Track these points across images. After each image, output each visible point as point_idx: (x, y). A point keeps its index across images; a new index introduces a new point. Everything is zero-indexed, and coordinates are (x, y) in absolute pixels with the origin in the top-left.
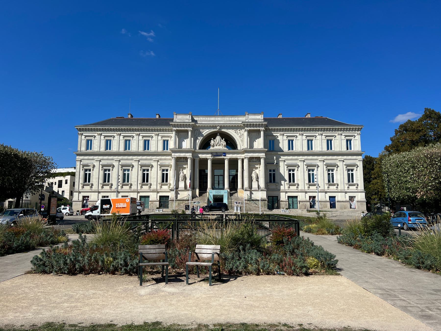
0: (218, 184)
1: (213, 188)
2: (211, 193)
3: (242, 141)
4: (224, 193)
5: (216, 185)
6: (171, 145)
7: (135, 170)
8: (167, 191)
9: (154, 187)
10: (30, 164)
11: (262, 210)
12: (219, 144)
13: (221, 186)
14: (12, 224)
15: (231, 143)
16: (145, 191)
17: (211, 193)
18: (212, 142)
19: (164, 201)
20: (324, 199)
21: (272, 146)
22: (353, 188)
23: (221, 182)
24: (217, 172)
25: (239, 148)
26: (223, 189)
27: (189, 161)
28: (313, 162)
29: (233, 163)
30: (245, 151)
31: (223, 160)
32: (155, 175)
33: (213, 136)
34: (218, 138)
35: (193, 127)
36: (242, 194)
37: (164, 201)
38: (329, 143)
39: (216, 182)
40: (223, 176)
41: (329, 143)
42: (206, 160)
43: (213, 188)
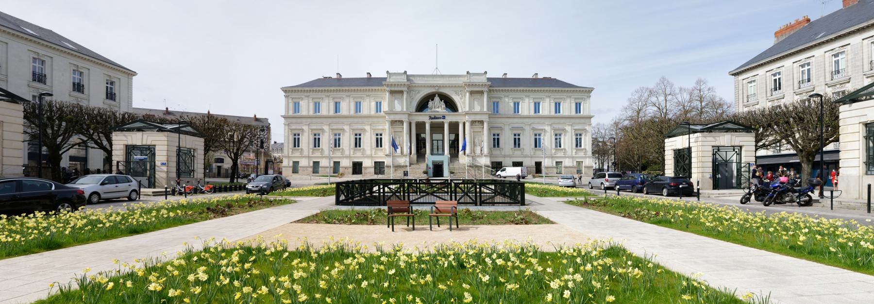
0: (437, 149)
1: (432, 154)
2: (430, 159)
3: (464, 103)
4: (445, 158)
5: (435, 151)
6: (385, 107)
7: (548, 135)
8: (383, 155)
9: (347, 153)
10: (791, 108)
11: (484, 176)
12: (438, 107)
13: (440, 152)
14: (386, 285)
15: (451, 105)
16: (337, 155)
17: (430, 159)
18: (430, 103)
19: (379, 167)
20: (571, 165)
21: (495, 107)
22: (581, 154)
23: (440, 147)
24: (437, 136)
25: (460, 110)
26: (443, 154)
27: (405, 125)
28: (560, 126)
29: (454, 127)
30: (467, 114)
31: (443, 124)
32: (368, 140)
33: (431, 97)
34: (437, 99)
35: (409, 87)
36: (463, 160)
37: (379, 167)
38: (557, 107)
39: (435, 147)
40: (443, 141)
41: (557, 107)
42: (424, 124)
43: (432, 154)
